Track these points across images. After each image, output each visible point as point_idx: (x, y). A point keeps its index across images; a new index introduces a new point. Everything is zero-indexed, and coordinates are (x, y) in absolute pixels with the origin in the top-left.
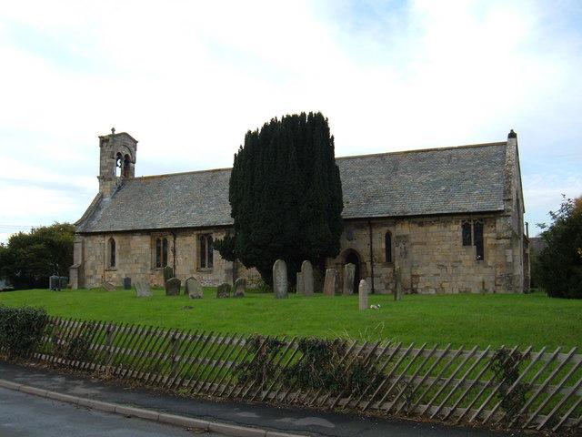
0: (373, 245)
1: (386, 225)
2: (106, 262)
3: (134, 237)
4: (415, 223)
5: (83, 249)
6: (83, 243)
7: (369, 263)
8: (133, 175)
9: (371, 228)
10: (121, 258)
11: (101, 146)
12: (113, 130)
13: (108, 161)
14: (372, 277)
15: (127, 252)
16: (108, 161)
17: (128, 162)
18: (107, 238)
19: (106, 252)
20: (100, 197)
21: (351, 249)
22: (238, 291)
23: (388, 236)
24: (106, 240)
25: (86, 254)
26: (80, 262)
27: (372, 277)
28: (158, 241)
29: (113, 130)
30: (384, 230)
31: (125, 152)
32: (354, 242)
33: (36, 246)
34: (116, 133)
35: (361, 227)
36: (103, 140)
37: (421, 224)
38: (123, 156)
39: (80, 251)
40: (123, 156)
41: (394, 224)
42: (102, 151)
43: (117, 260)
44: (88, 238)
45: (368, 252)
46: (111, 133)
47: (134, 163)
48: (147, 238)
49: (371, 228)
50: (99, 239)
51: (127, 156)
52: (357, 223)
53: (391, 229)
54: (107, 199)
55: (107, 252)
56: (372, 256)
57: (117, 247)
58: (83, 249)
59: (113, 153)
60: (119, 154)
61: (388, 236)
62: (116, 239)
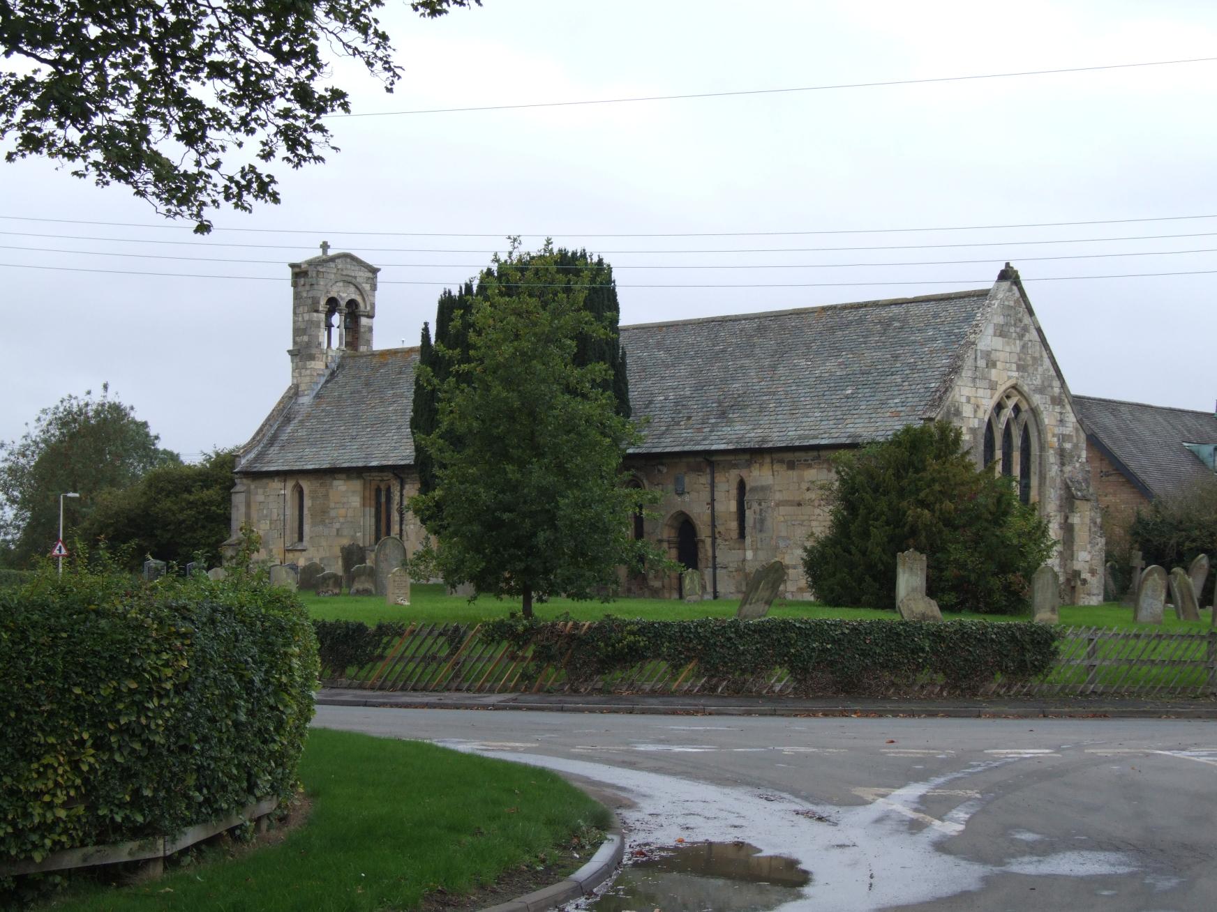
0: (717, 506)
1: (735, 466)
2: (288, 532)
3: (336, 483)
4: (781, 461)
5: (248, 505)
6: (248, 492)
7: (709, 541)
8: (368, 342)
9: (713, 474)
10: (314, 525)
11: (295, 285)
12: (325, 246)
13: (306, 317)
14: (715, 568)
15: (322, 515)
16: (306, 317)
17: (355, 316)
18: (290, 484)
19: (288, 512)
20: (294, 393)
21: (682, 513)
22: (358, 586)
23: (742, 486)
24: (287, 489)
25: (254, 515)
26: (1037, 499)
27: (715, 568)
28: (378, 490)
29: (325, 246)
30: (733, 475)
31: (346, 295)
32: (687, 498)
33: (198, 495)
34: (331, 253)
35: (698, 469)
36: (300, 273)
37: (791, 466)
38: (343, 303)
39: (243, 509)
40: (343, 303)
41: (749, 464)
42: (297, 296)
43: (306, 528)
44: (257, 483)
45: (706, 517)
46: (319, 253)
47: (371, 317)
48: (356, 485)
49: (713, 474)
50: (276, 485)
51: (352, 303)
52: (691, 460)
53: (744, 473)
54: (306, 400)
55: (291, 512)
56: (714, 526)
57: (307, 503)
58: (248, 505)
59: (315, 301)
60: (333, 304)
61: (742, 486)
62: (306, 485)
